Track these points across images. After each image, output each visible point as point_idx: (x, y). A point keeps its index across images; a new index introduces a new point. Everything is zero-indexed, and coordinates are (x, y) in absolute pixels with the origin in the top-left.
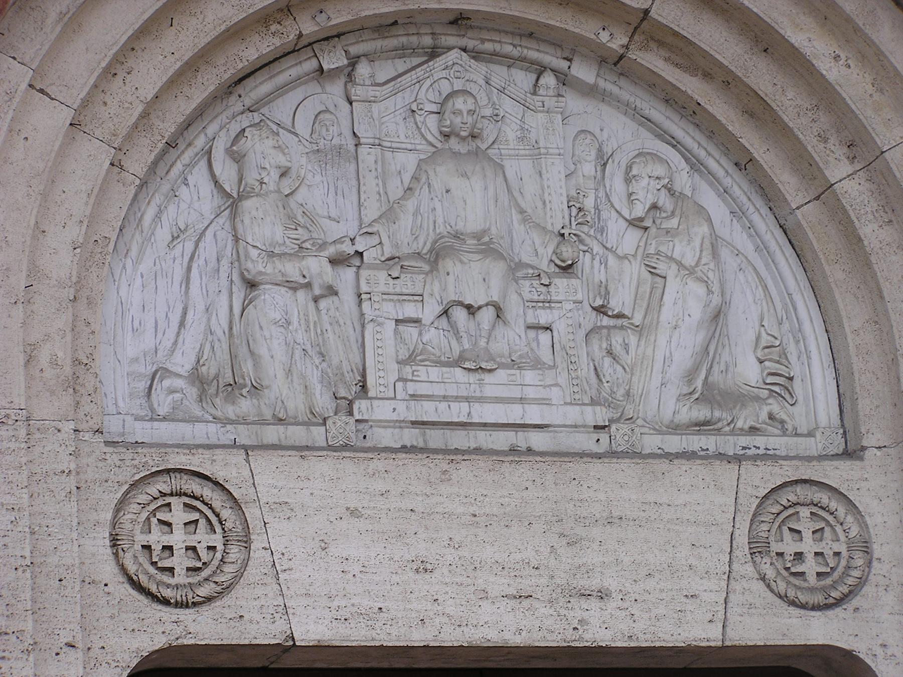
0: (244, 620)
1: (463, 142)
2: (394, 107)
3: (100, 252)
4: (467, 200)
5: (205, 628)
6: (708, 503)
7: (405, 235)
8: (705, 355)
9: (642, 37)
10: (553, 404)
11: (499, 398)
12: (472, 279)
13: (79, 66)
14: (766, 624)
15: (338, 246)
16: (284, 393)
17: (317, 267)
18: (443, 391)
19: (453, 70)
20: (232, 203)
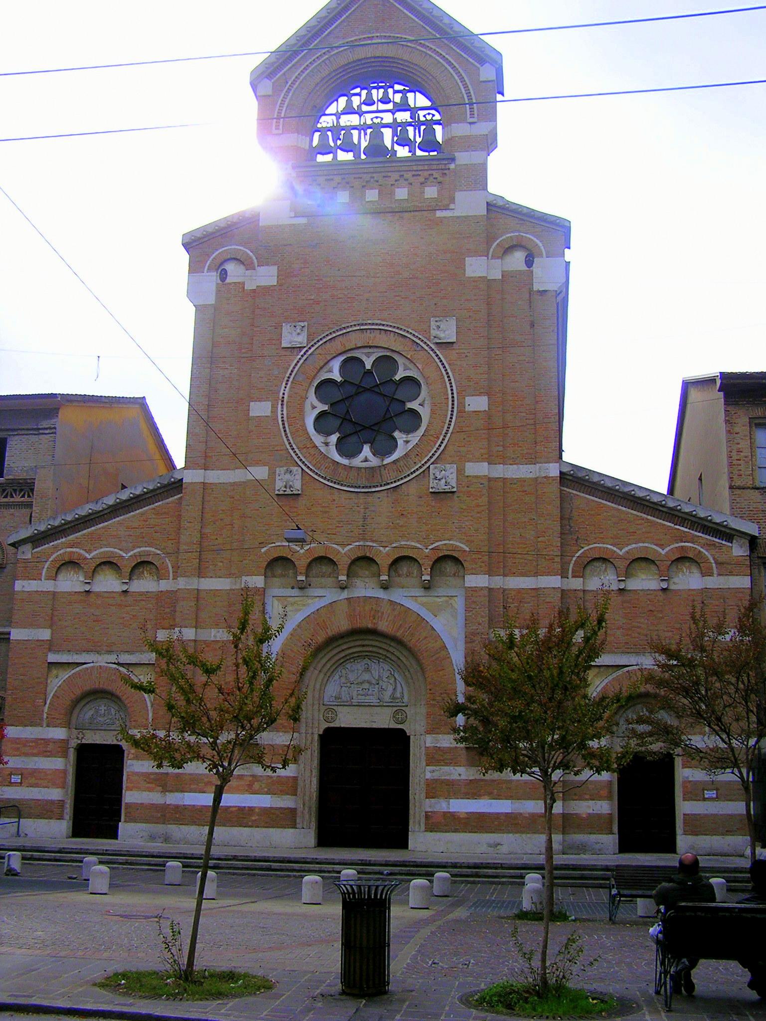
0: (336, 724)
1: (367, 670)
2: (359, 666)
3: (324, 685)
4: (366, 676)
5: (332, 725)
6: (389, 711)
7: (359, 680)
8: (393, 694)
9: (486, 703)
10: (374, 700)
11: (368, 699)
12: (366, 686)
13: (320, 666)
14: (394, 725)
15: (365, 588)
16: (344, 699)
17: (349, 685)
18: (362, 699)
19: (367, 661)
20: (341, 677)
